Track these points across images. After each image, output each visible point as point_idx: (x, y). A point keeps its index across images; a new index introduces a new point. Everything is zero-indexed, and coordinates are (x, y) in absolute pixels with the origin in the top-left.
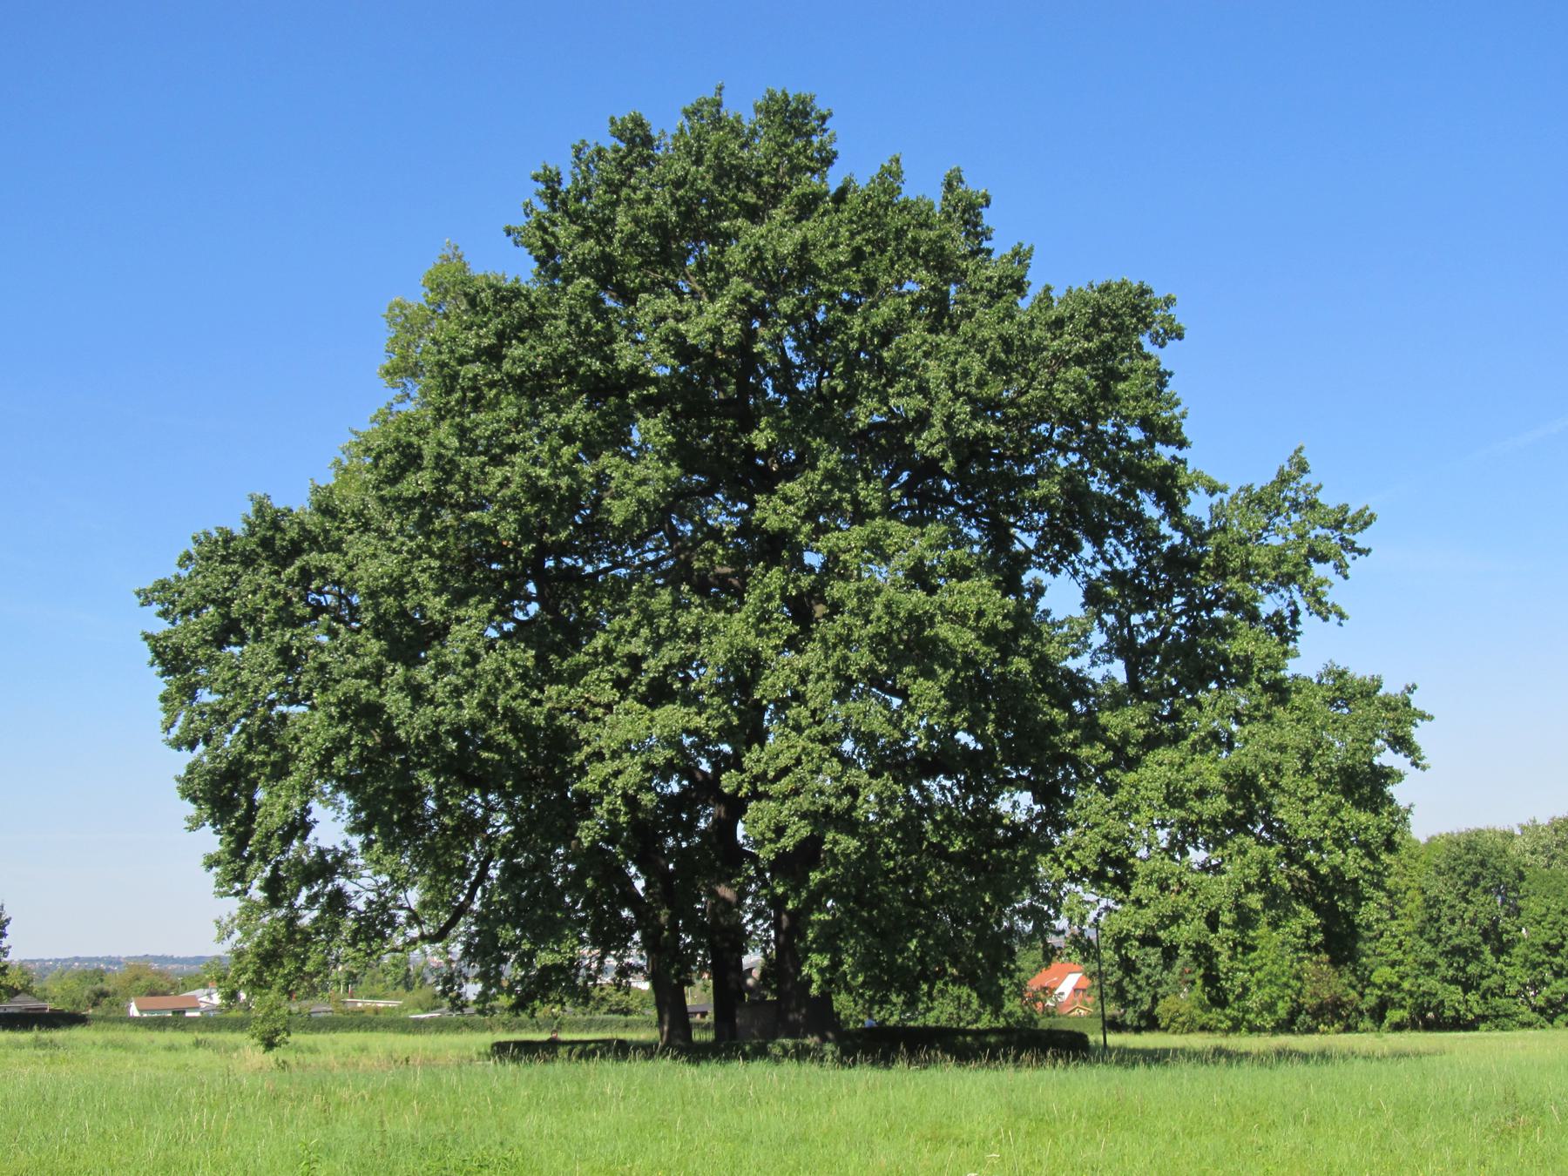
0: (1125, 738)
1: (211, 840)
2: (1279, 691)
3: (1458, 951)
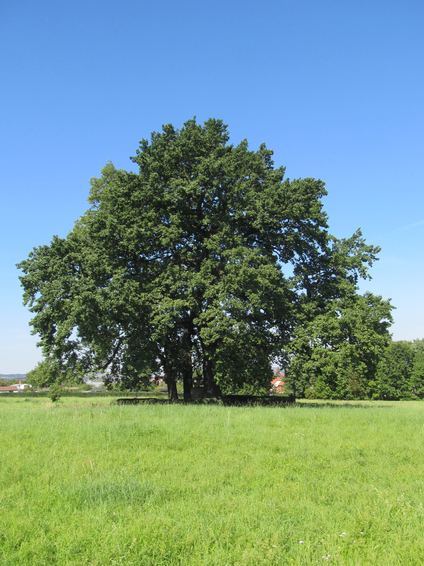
0: (309, 312)
1: (37, 338)
2: (354, 299)
3: (394, 377)
